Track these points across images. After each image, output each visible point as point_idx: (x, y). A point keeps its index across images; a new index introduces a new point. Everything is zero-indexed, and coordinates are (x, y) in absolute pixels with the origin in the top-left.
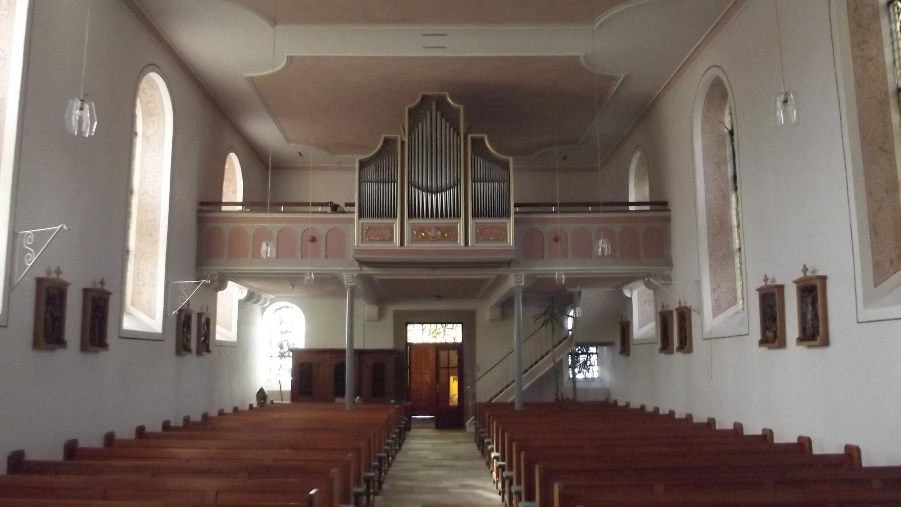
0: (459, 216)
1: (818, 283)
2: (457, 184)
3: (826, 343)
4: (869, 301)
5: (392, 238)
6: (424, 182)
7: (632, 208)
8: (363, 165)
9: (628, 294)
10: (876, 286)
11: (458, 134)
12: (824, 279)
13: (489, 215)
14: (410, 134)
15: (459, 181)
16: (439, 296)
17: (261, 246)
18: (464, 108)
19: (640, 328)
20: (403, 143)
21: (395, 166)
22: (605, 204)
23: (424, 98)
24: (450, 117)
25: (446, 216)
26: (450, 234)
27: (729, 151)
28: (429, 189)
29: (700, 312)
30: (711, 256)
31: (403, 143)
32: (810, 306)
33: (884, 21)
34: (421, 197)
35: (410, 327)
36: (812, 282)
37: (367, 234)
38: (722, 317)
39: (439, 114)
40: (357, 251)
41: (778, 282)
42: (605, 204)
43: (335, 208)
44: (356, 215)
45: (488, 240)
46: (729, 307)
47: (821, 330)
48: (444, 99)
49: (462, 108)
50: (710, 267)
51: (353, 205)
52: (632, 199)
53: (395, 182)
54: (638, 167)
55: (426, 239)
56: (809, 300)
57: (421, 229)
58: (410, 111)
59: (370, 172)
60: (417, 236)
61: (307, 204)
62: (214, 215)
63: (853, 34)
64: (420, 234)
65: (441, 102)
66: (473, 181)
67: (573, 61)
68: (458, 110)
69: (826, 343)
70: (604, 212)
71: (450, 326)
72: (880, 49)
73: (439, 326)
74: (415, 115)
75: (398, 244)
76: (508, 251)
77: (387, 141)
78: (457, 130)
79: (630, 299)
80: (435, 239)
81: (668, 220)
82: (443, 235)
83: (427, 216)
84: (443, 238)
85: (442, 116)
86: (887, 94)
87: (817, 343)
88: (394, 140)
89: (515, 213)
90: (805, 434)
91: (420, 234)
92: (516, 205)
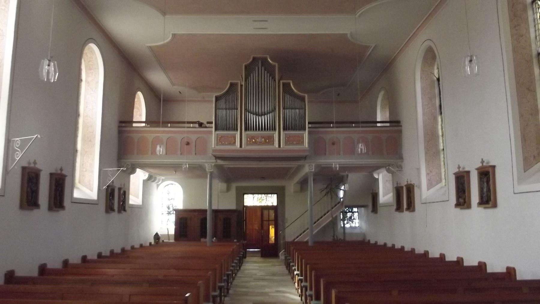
0: (275, 130)
1: (490, 170)
2: (274, 110)
3: (495, 206)
4: (521, 180)
5: (235, 143)
6: (254, 109)
7: (379, 125)
8: (217, 99)
9: (376, 176)
10: (525, 172)
11: (275, 80)
12: (494, 167)
13: (293, 129)
14: (246, 81)
15: (275, 108)
16: (263, 178)
17: (156, 147)
18: (278, 65)
19: (384, 196)
20: (241, 86)
21: (237, 99)
22: (363, 122)
23: (254, 59)
24: (270, 70)
25: (268, 130)
26: (269, 140)
27: (437, 91)
28: (257, 113)
29: (420, 187)
30: (426, 153)
31: (241, 86)
32: (485, 184)
33: (530, 13)
34: (253, 118)
35: (246, 196)
36: (487, 169)
37: (220, 140)
38: (432, 190)
39: (263, 68)
40: (214, 151)
41: (467, 169)
42: (363, 122)
43: (201, 125)
44: (213, 129)
45: (292, 144)
46: (437, 184)
47: (492, 198)
48: (266, 59)
49: (277, 65)
50: (426, 160)
51: (211, 123)
52: (379, 119)
53: (237, 109)
54: (382, 100)
55: (255, 143)
56: (485, 180)
57: (253, 137)
58: (246, 66)
59: (222, 103)
60: (250, 141)
61: (184, 123)
62: (128, 129)
63: (511, 20)
64: (251, 140)
65: (264, 61)
66: (284, 108)
67: (343, 37)
68: (274, 66)
69: (495, 206)
70: (362, 127)
71: (270, 195)
72: (528, 30)
73: (263, 195)
74: (249, 69)
75: (239, 146)
76: (304, 151)
77: (232, 85)
78: (274, 78)
79: (378, 179)
80: (261, 143)
81: (400, 132)
82: (265, 141)
83: (256, 129)
84: (265, 143)
85: (265, 70)
86: (531, 56)
87: (490, 205)
88: (236, 84)
89: (309, 128)
90: (483, 260)
91: (251, 140)
92: (309, 123)
